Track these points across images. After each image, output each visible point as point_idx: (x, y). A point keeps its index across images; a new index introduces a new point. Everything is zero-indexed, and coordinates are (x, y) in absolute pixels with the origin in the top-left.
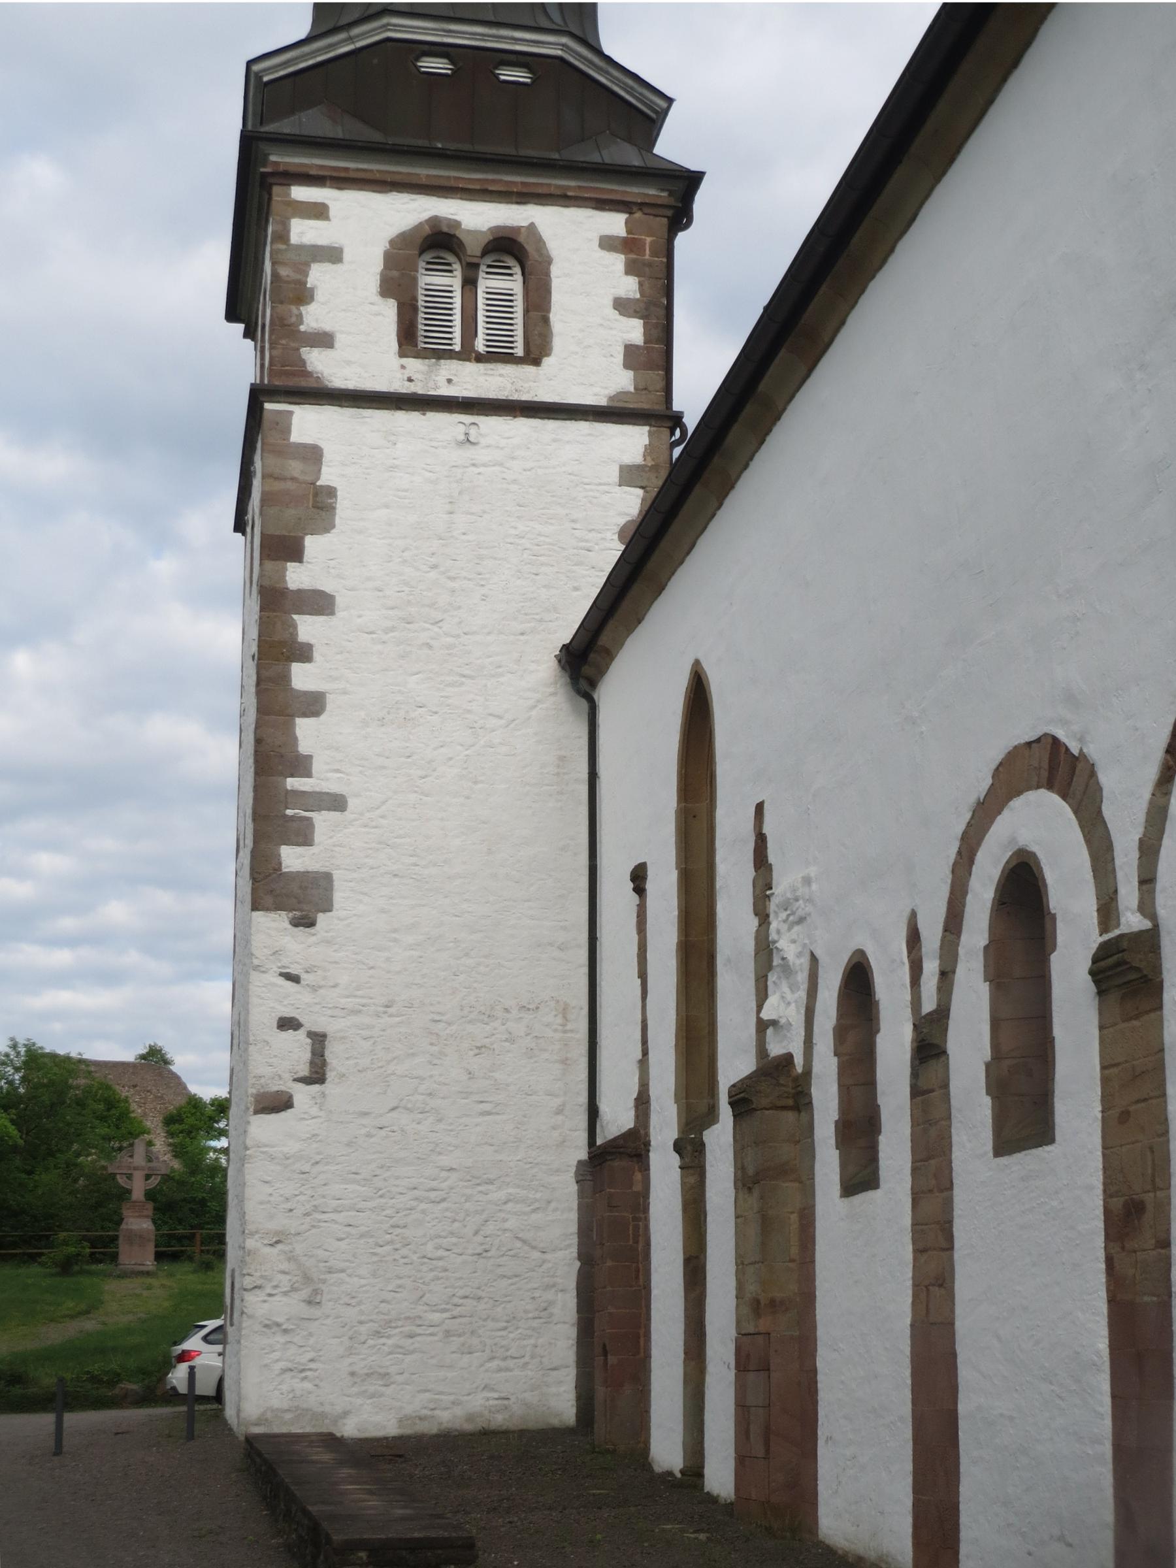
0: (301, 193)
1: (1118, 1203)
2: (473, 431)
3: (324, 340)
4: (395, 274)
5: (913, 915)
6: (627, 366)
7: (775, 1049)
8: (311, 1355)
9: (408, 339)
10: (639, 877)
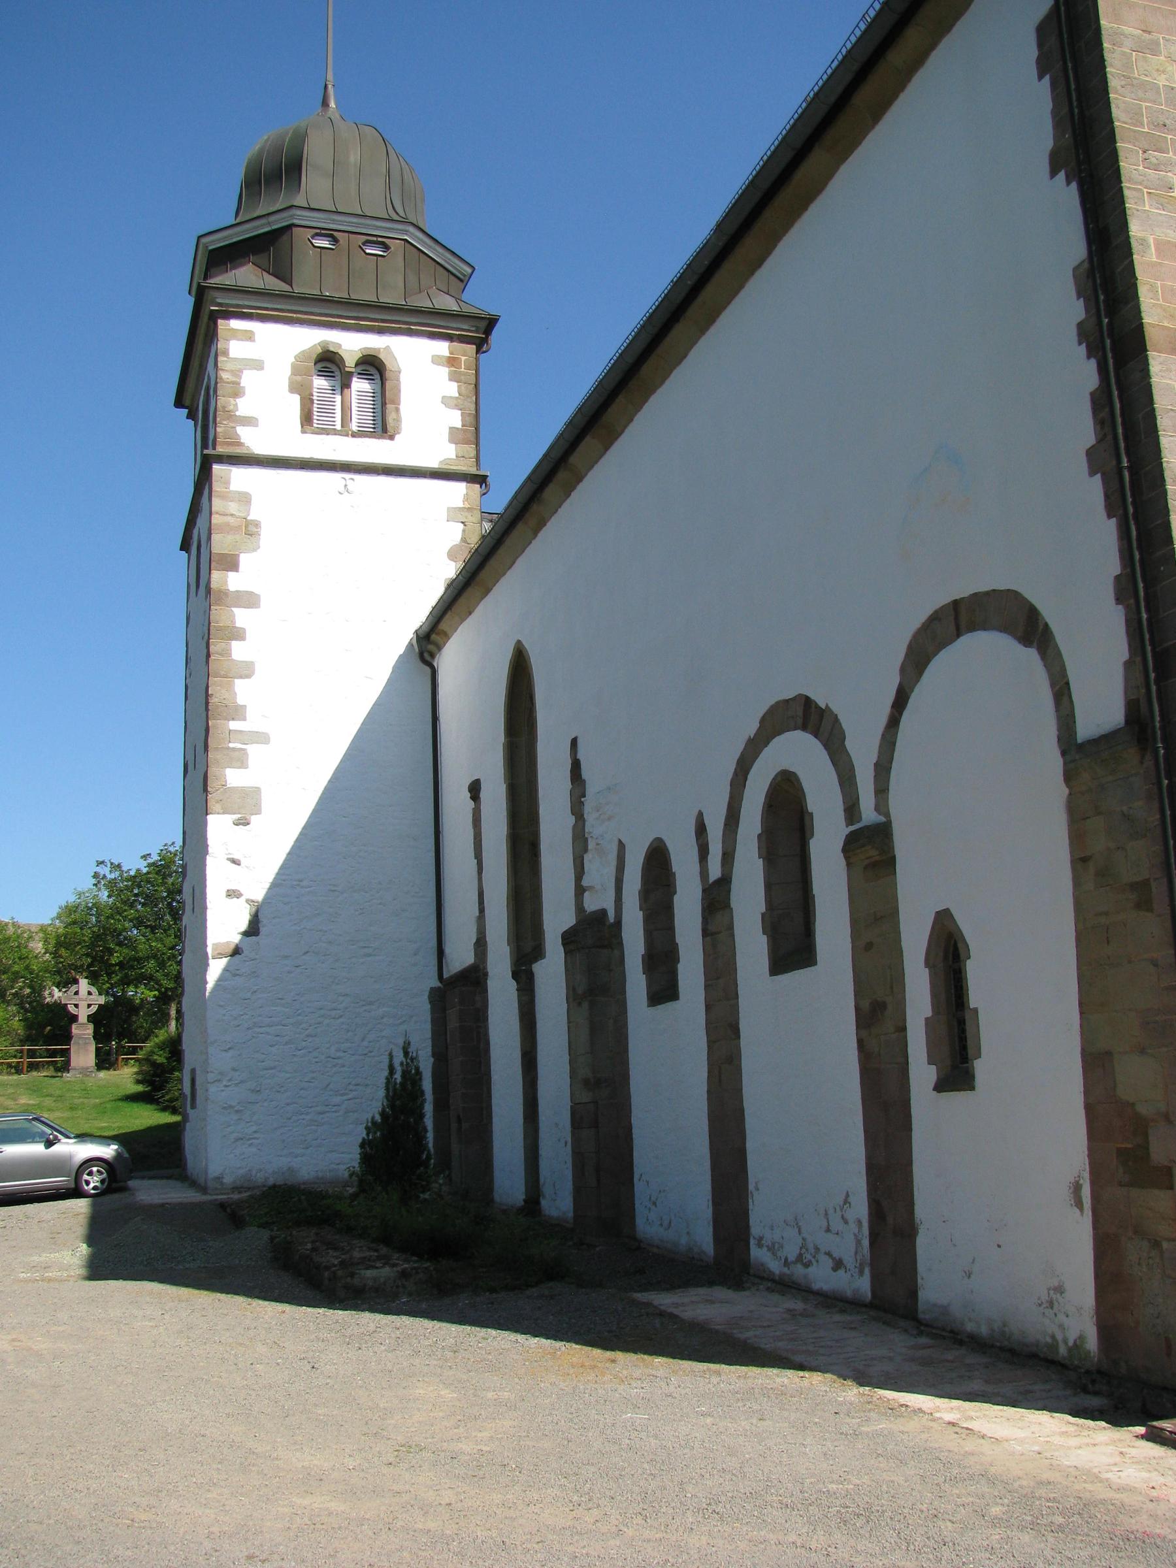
0: (235, 324)
1: (866, 1004)
2: (349, 483)
3: (250, 421)
4: (299, 378)
5: (700, 814)
6: (451, 441)
7: (591, 904)
8: (254, 1128)
9: (307, 419)
10: (475, 789)
